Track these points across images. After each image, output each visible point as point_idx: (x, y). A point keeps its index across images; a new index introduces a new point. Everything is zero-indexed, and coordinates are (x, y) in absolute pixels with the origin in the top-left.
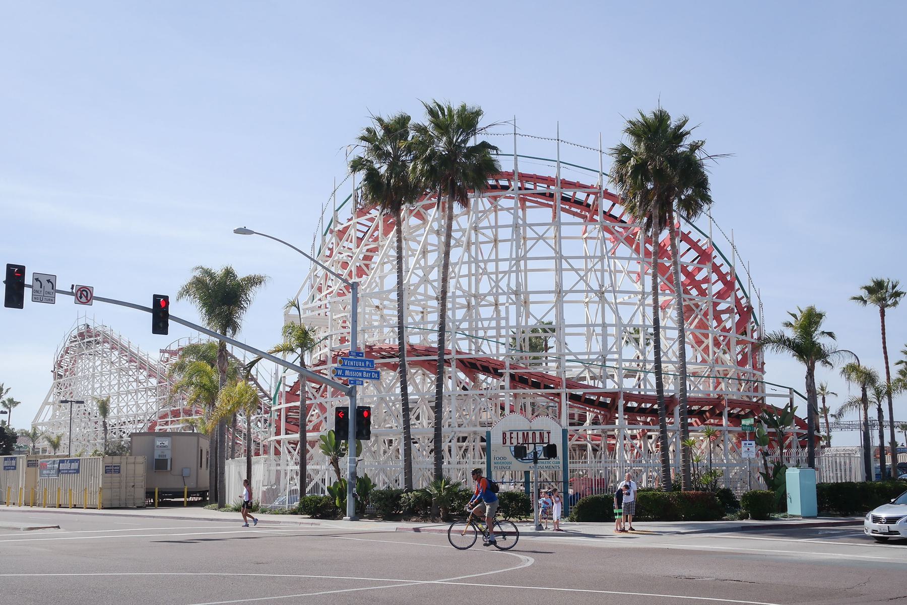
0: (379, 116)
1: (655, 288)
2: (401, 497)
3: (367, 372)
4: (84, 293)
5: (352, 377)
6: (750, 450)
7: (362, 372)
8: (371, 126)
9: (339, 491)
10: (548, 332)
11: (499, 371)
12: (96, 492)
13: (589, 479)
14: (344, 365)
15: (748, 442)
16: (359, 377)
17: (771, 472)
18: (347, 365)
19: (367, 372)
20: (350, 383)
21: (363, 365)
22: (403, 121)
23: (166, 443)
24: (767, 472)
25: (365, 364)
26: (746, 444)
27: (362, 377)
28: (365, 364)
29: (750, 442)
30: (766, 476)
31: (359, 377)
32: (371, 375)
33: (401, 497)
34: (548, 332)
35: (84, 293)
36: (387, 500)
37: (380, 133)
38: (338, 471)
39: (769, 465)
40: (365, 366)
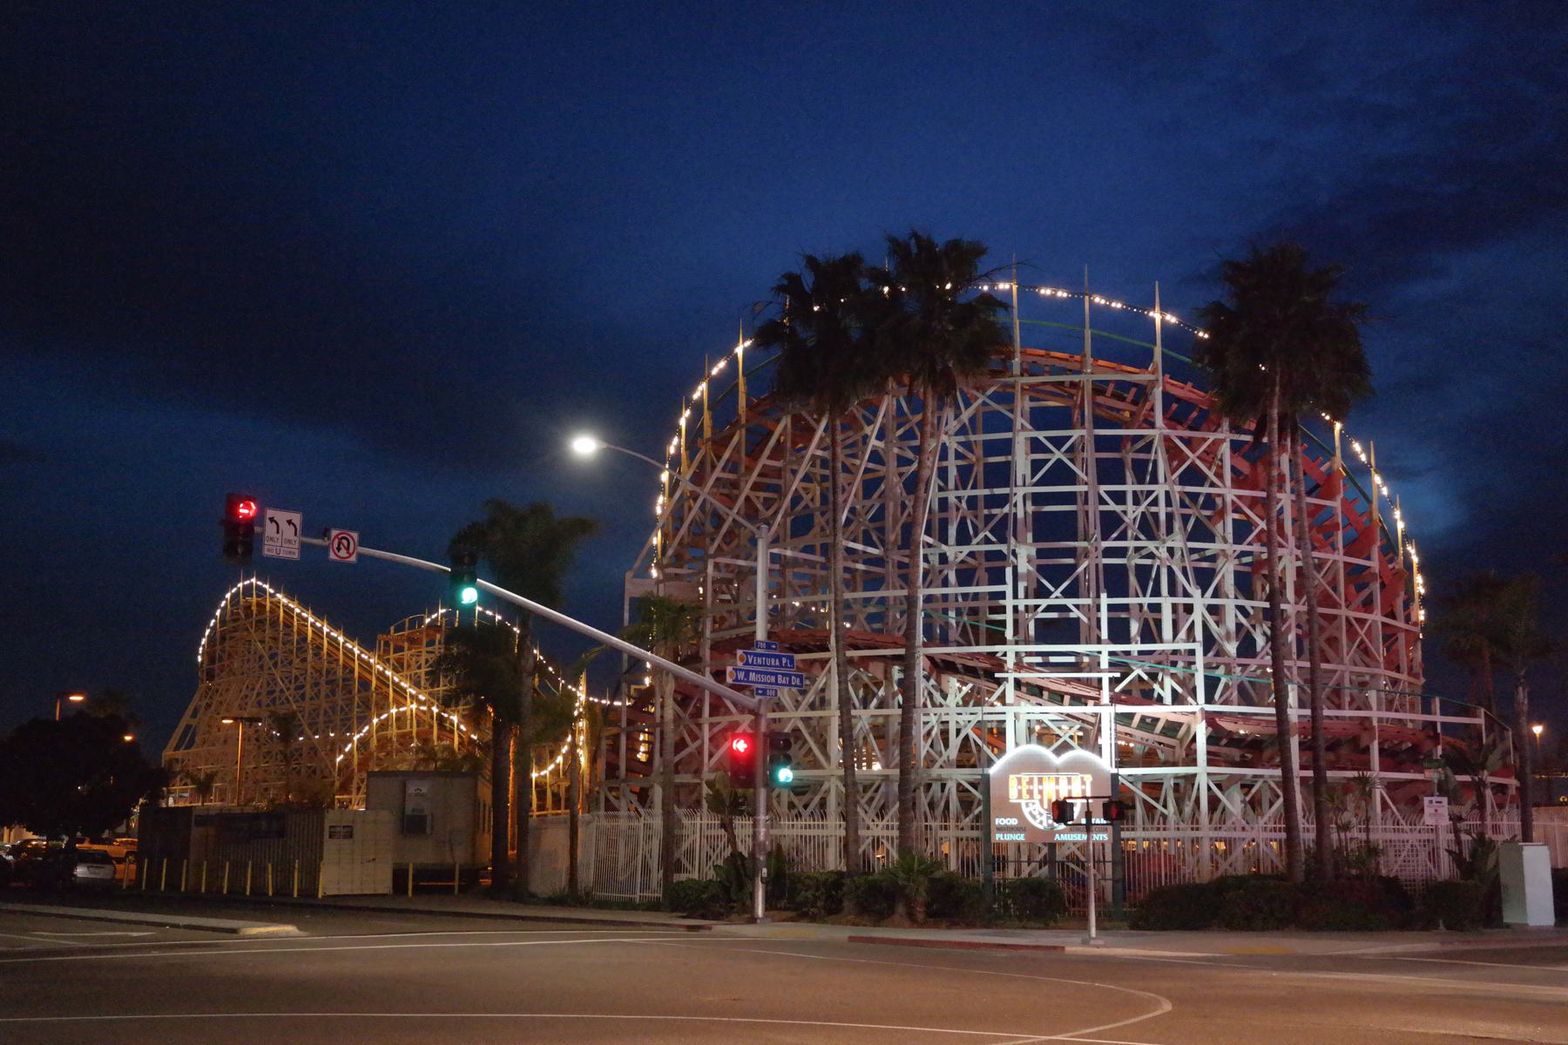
0: (812, 253)
1: (835, 493)
2: (843, 884)
3: (783, 675)
4: (345, 542)
5: (760, 683)
6: (1437, 811)
7: (776, 675)
8: (796, 270)
9: (738, 871)
10: (1193, 622)
11: (997, 675)
12: (917, 838)
13: (1139, 855)
14: (747, 663)
15: (1434, 799)
16: (770, 684)
17: (1466, 854)
18: (752, 664)
19: (783, 675)
20: (758, 694)
21: (778, 663)
22: (851, 263)
23: (424, 790)
24: (1461, 850)
25: (781, 662)
26: (1431, 802)
27: (776, 683)
28: (781, 662)
29: (1439, 799)
30: (1456, 857)
31: (770, 684)
32: (790, 681)
33: (843, 884)
34: (1193, 622)
35: (345, 542)
36: (817, 890)
37: (808, 280)
38: (732, 840)
39: (1464, 837)
40: (781, 666)
